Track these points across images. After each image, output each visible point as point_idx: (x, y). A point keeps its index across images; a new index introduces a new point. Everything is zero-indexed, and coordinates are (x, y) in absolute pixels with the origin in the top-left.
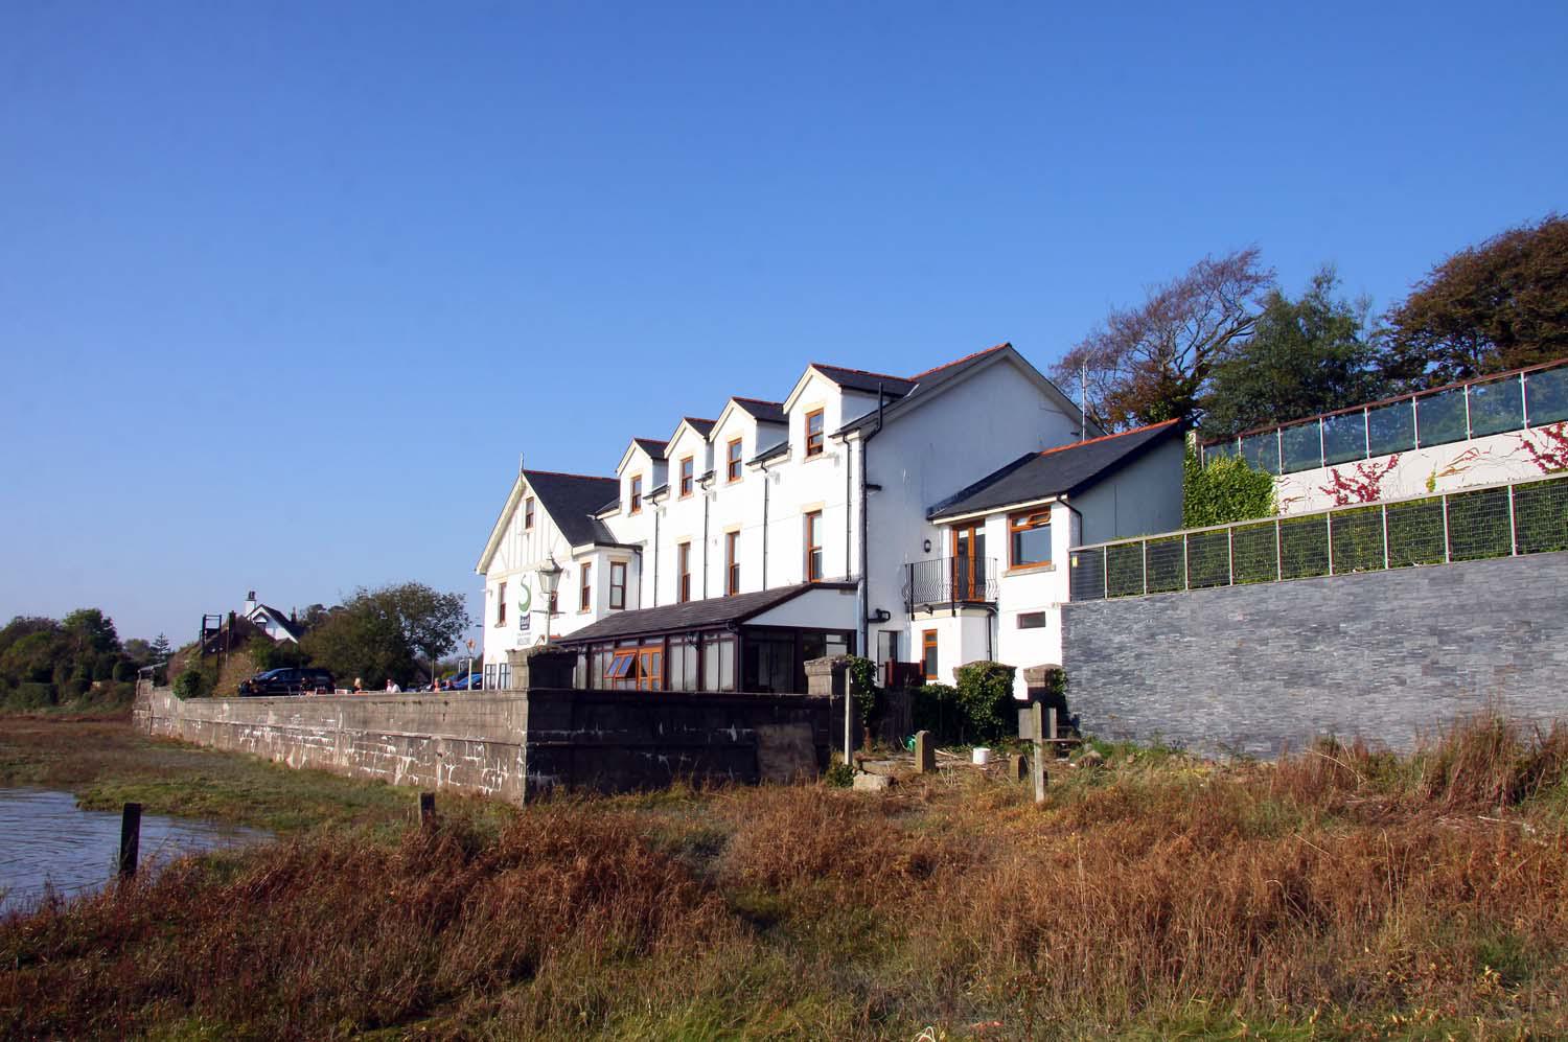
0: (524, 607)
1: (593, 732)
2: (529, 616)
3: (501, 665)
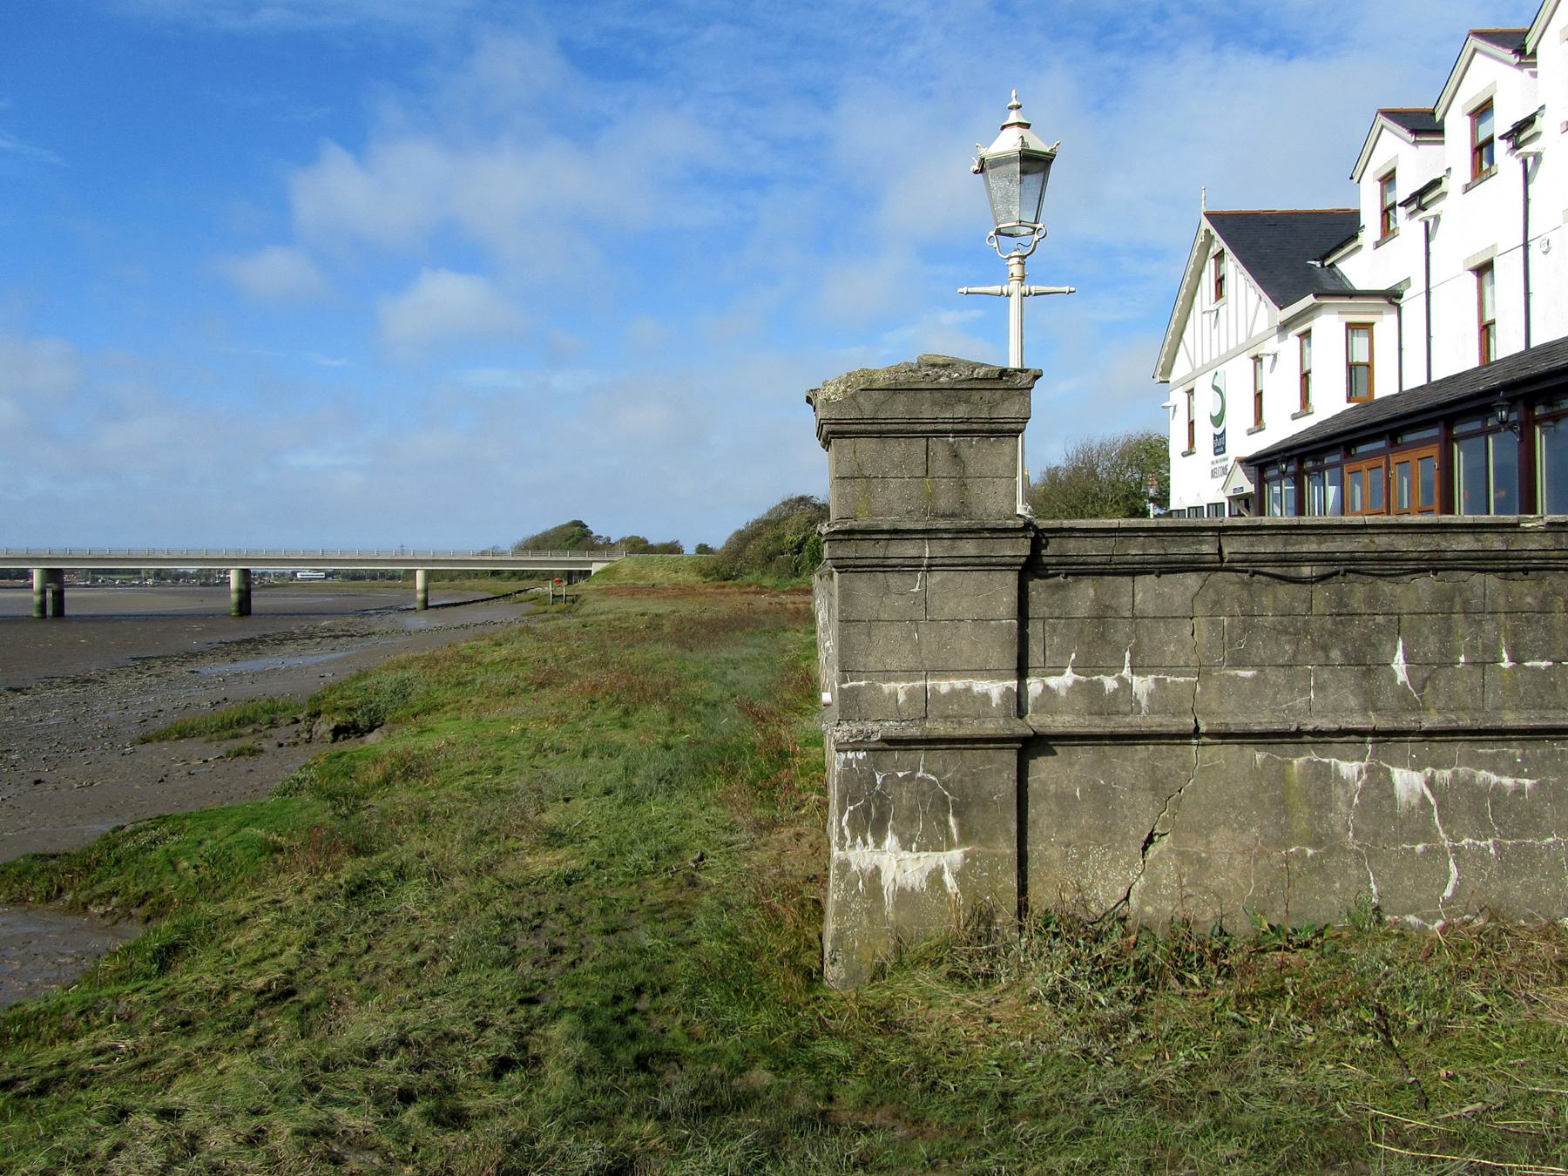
0: (1217, 420)
1: (1110, 683)
2: (1224, 432)
3: (1208, 505)
